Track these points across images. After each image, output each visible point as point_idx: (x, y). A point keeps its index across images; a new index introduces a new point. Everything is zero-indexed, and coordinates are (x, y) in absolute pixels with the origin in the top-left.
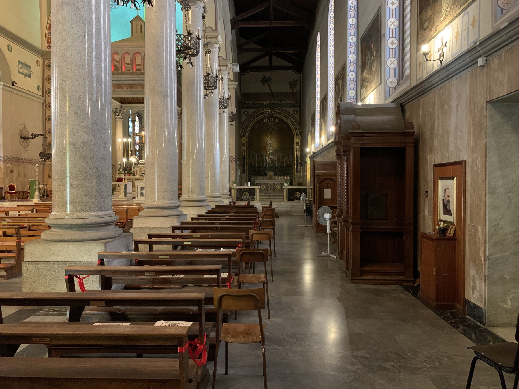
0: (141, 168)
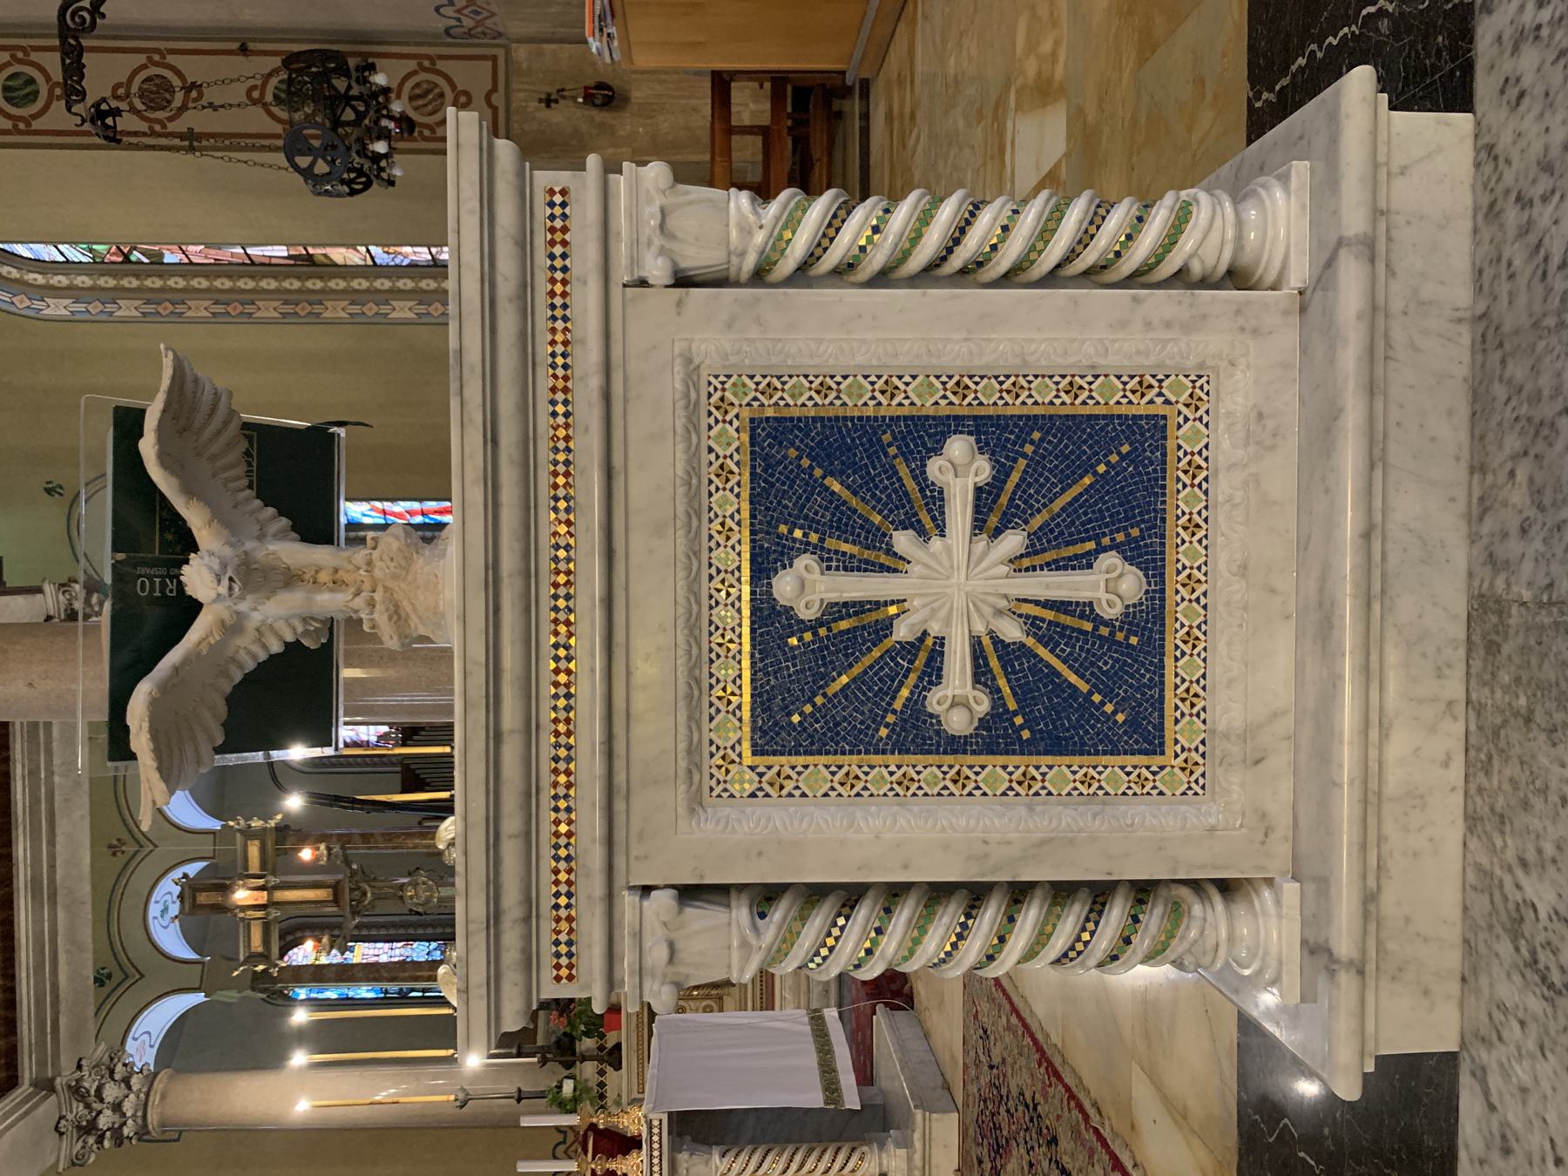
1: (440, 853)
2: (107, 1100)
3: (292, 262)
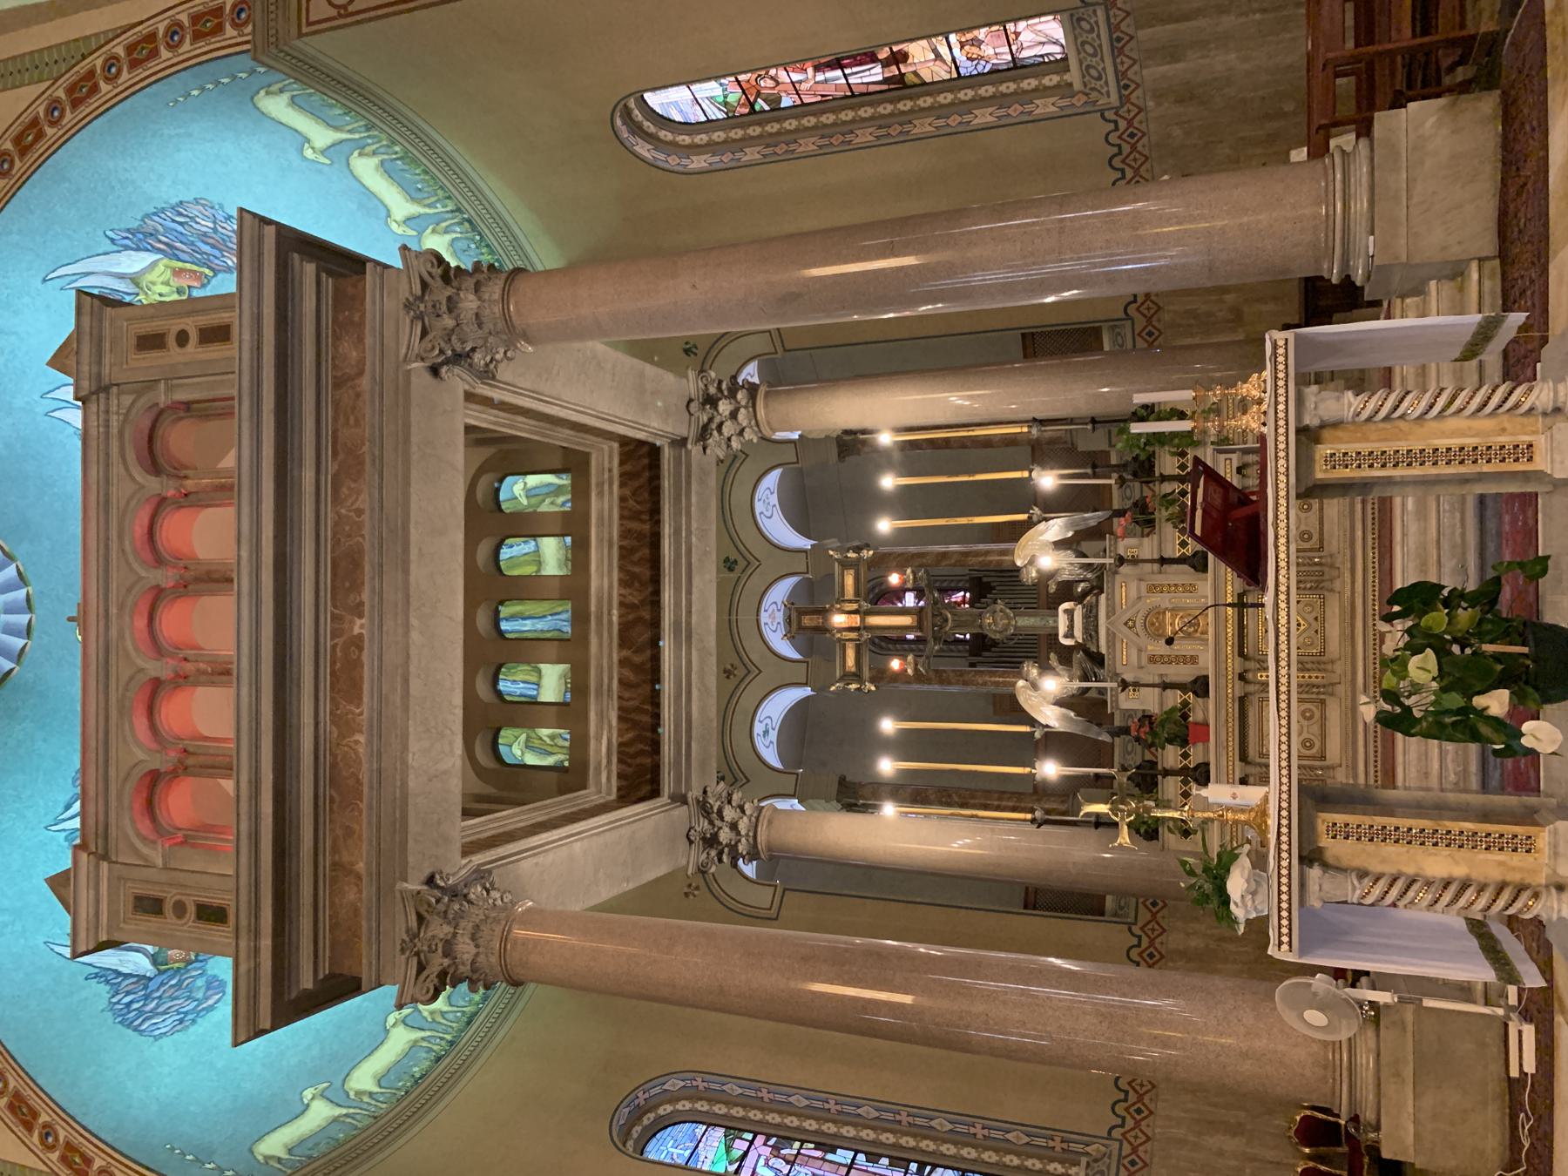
1: (1018, 570)
2: (726, 819)
3: (885, 87)
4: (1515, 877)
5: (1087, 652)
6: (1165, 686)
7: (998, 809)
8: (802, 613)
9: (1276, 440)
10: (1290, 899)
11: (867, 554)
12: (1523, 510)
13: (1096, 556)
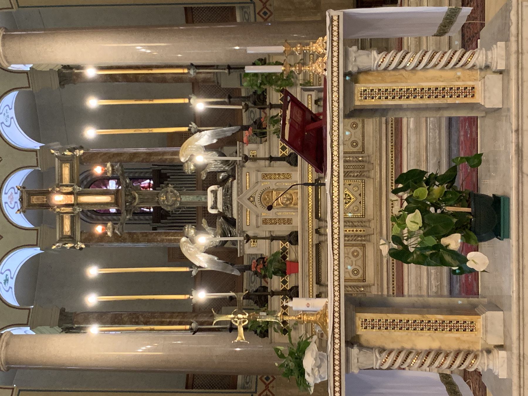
0: (251, 199)
4: (465, 347)
5: (226, 218)
6: (273, 238)
7: (170, 324)
8: (30, 194)
9: (332, 80)
10: (340, 369)
11: (79, 153)
12: (470, 126)
13: (231, 155)
